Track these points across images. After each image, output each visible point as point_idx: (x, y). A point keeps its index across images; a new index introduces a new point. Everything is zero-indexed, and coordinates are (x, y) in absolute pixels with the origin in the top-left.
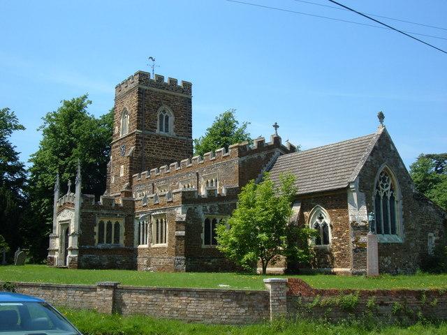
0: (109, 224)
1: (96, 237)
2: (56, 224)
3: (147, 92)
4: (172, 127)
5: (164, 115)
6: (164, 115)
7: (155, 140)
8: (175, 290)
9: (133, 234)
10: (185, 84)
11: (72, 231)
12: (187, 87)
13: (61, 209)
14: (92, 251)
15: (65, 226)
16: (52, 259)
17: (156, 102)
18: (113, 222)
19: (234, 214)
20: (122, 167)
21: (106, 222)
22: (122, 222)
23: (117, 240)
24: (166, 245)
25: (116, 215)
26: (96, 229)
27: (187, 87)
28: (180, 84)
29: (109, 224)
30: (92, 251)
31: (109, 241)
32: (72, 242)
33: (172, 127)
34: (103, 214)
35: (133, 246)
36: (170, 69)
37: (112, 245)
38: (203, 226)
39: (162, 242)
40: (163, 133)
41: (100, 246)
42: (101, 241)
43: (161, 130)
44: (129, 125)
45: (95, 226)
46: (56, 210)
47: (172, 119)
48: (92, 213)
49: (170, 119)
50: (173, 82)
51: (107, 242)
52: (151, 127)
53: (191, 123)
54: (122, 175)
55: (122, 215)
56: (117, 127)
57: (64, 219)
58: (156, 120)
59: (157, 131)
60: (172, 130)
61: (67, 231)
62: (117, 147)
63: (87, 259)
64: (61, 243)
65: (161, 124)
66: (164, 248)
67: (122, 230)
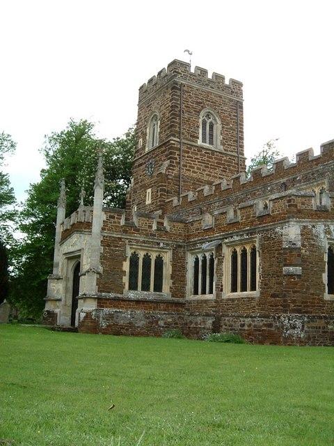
0: (147, 260)
1: (126, 280)
2: (59, 258)
3: (185, 88)
4: (218, 138)
5: (209, 121)
6: (209, 121)
7: (197, 154)
8: (118, 333)
9: (184, 276)
10: (233, 82)
11: (85, 266)
12: (236, 86)
13: (67, 234)
14: (117, 302)
15: (75, 258)
16: (52, 315)
17: (198, 103)
18: (153, 256)
19: (85, 314)
20: (149, 191)
21: (141, 255)
22: (167, 258)
23: (158, 287)
24: (256, 294)
25: (159, 244)
26: (126, 266)
27: (236, 86)
28: (227, 82)
29: (147, 260)
30: (117, 302)
31: (146, 287)
32: (88, 285)
33: (218, 138)
34: (138, 241)
35: (183, 296)
36: (211, 60)
37: (151, 294)
38: (326, 259)
39: (244, 289)
40: (207, 145)
41: (132, 295)
42: (133, 286)
43: (204, 141)
44: (160, 133)
45: (125, 260)
46: (58, 237)
47: (218, 127)
48: (120, 239)
49: (215, 127)
50: (219, 78)
51: (155, 290)
52: (191, 136)
53: (242, 135)
54: (148, 202)
55: (167, 245)
56: (141, 140)
57: (71, 249)
58: (198, 127)
59: (200, 142)
60: (219, 143)
61: (77, 268)
62: (141, 165)
63: (111, 316)
64: (66, 289)
65: (204, 134)
66: (251, 299)
67: (167, 270)
